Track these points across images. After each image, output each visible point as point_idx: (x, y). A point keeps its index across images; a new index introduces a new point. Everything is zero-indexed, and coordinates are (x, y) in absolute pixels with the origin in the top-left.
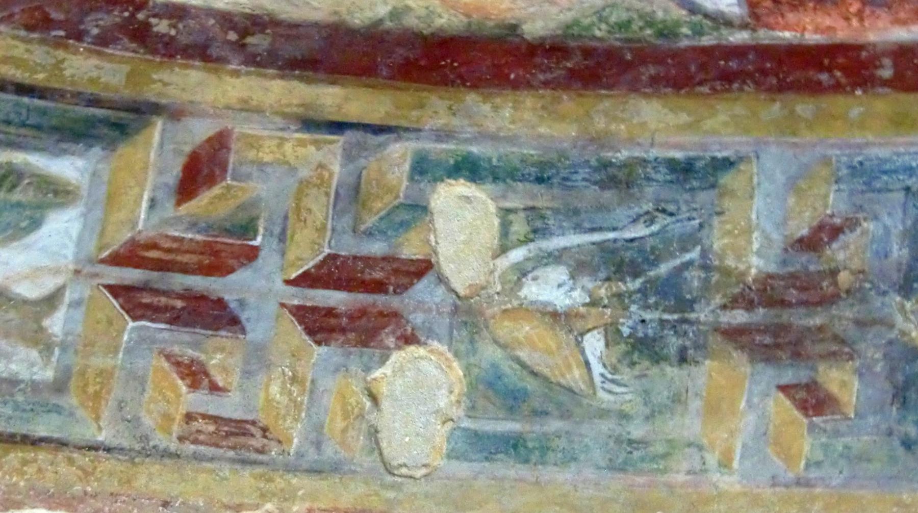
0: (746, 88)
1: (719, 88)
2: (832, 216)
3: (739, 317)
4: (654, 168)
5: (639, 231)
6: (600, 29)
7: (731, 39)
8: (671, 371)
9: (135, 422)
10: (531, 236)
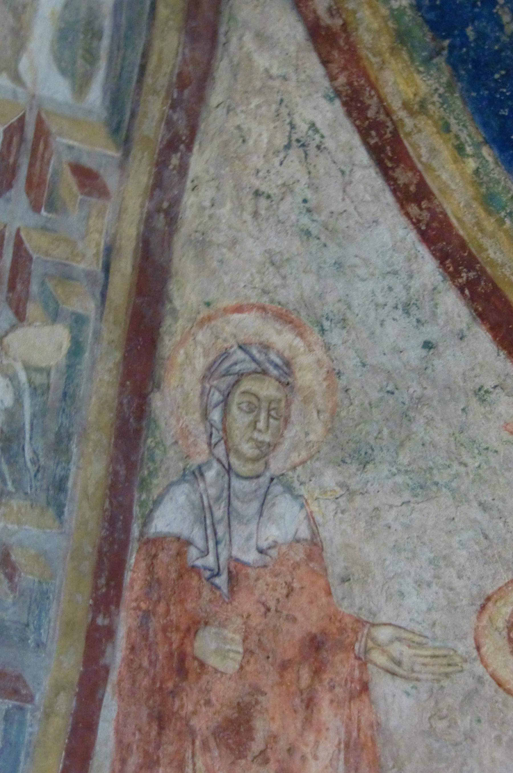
0: (104, 530)
1: (107, 513)
2: (20, 576)
4: (64, 468)
5: (28, 454)
6: (151, 442)
7: (135, 525)
10: (33, 386)
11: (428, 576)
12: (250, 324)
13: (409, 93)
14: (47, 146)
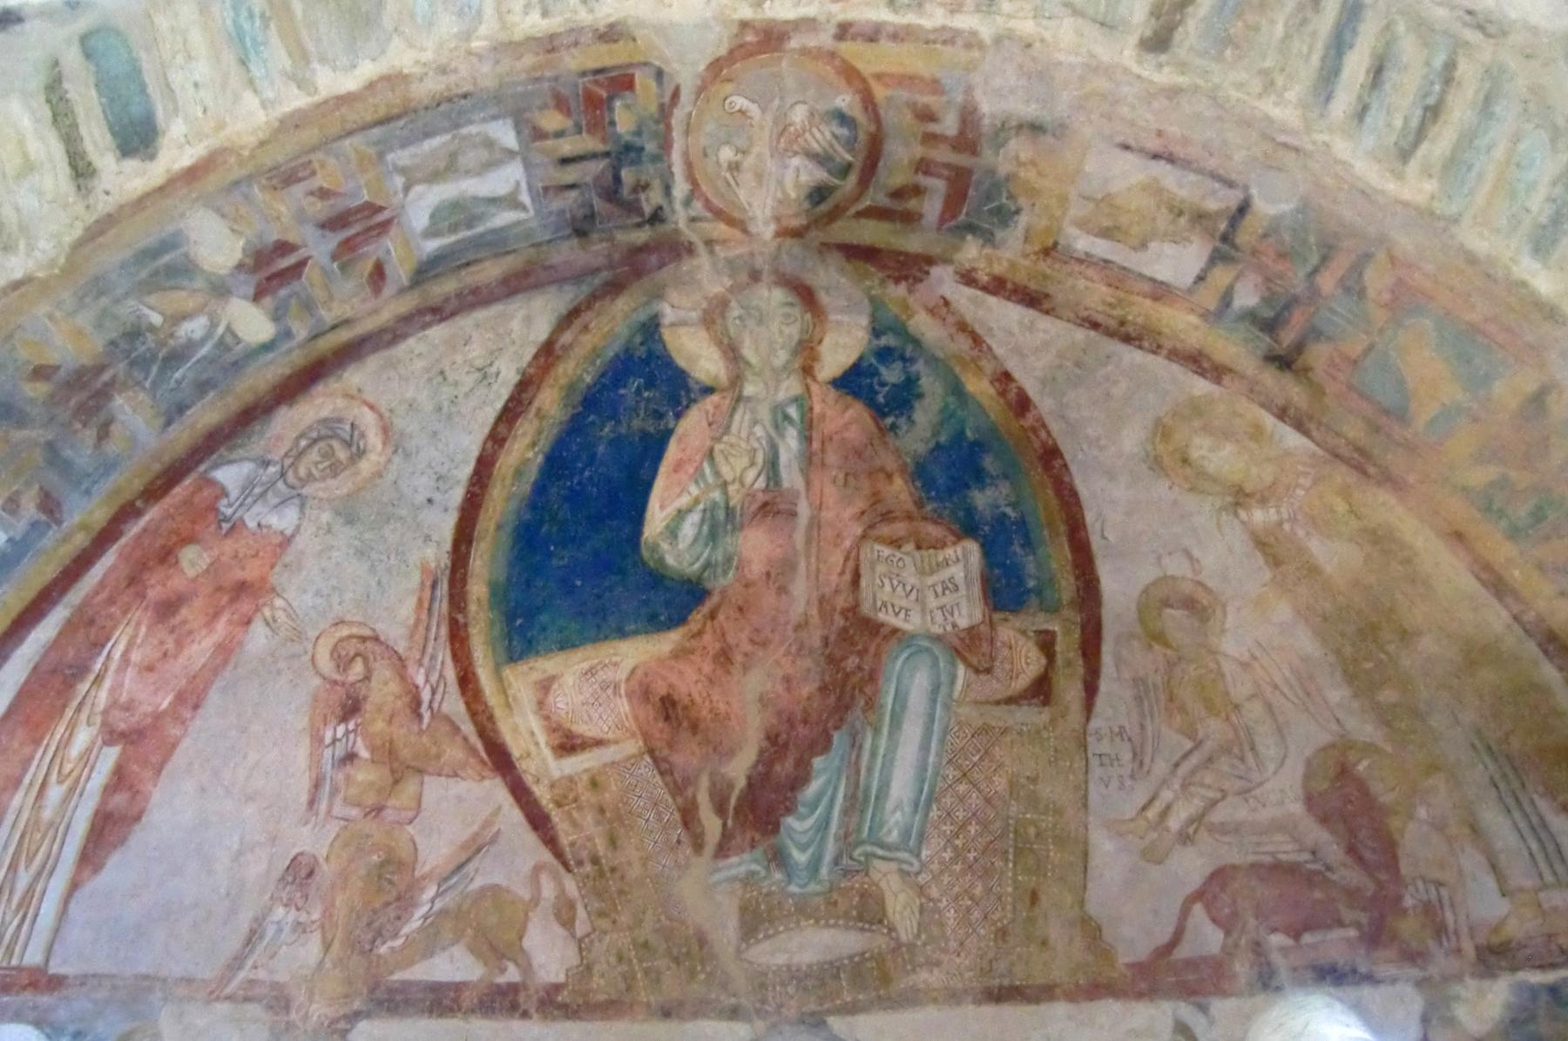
3: (106, 377)
5: (177, 375)
8: (114, 335)
9: (337, 157)
11: (325, 592)
12: (368, 419)
13: (546, 406)
14: (379, 235)
